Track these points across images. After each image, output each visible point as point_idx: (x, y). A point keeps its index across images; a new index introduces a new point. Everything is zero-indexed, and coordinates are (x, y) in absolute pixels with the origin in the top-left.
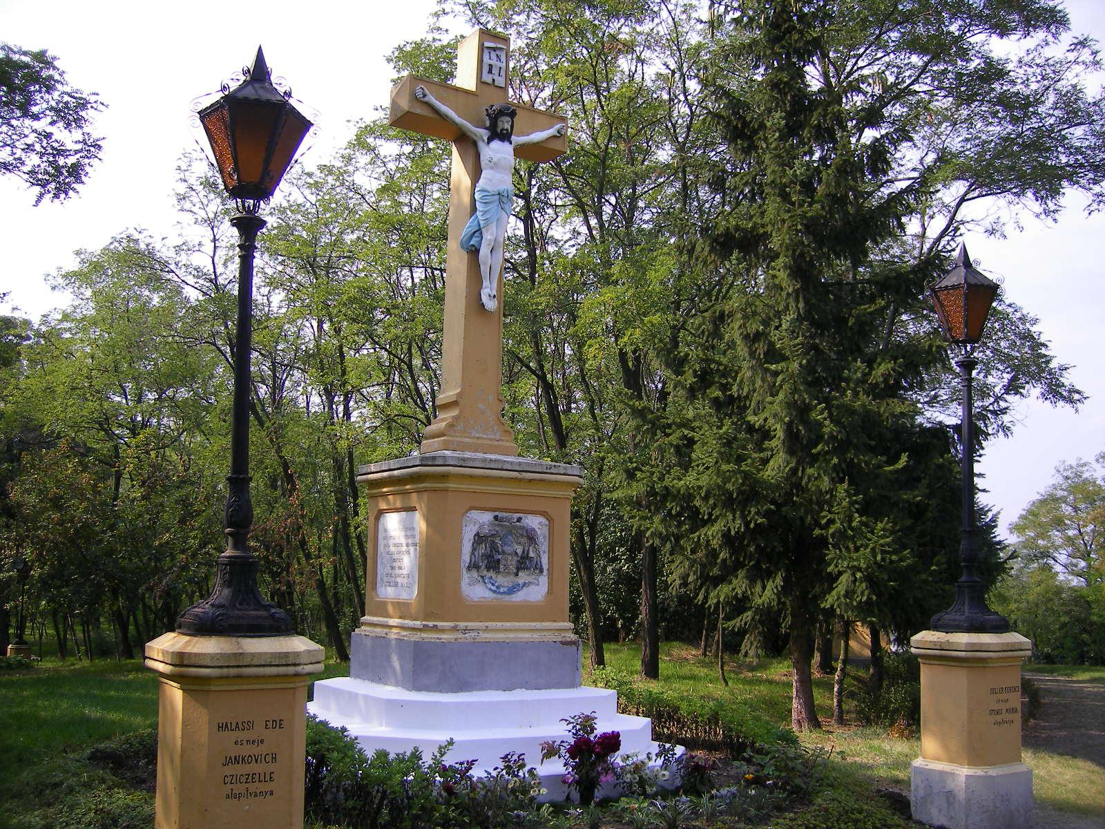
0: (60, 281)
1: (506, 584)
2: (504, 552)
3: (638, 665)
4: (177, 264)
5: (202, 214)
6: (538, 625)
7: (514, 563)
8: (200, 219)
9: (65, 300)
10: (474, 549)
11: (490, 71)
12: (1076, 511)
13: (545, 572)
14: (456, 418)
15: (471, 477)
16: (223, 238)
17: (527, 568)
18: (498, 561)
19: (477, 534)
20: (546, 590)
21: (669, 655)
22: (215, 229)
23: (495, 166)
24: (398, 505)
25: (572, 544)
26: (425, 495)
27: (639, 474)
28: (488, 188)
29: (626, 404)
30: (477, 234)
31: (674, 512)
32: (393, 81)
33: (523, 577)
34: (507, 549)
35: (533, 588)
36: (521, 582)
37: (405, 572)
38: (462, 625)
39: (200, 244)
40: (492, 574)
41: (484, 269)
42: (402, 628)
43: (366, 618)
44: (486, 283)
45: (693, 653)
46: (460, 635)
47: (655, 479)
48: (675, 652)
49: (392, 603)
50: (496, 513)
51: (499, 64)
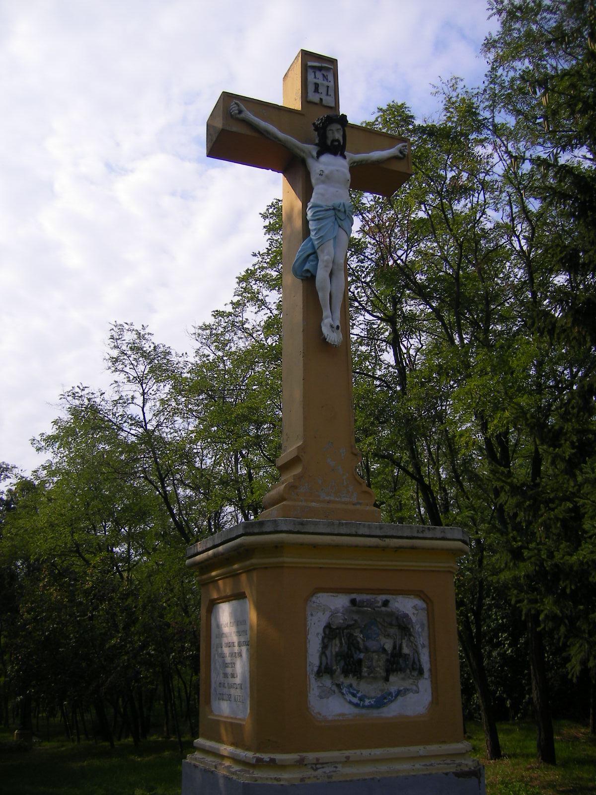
0: (43, 444)
1: (373, 694)
2: (367, 650)
3: (532, 746)
4: (114, 414)
5: (133, 373)
6: (420, 749)
7: (381, 663)
8: (132, 378)
9: (48, 456)
10: (325, 647)
11: (316, 90)
13: (426, 674)
14: (299, 478)
15: (315, 546)
16: (150, 391)
17: (401, 670)
18: (360, 661)
19: (328, 626)
20: (430, 699)
21: (559, 734)
22: (144, 386)
23: (327, 179)
24: (229, 592)
25: (459, 633)
26: (254, 574)
27: (526, 553)
28: (319, 203)
29: (503, 481)
30: (311, 258)
31: (568, 591)
33: (396, 682)
34: (372, 645)
35: (411, 697)
36: (393, 689)
37: (238, 680)
38: (311, 756)
39: (133, 398)
40: (351, 680)
41: (323, 297)
42: (236, 760)
43: (200, 741)
44: (326, 312)
45: (583, 730)
46: (310, 773)
47: (544, 557)
48: (565, 731)
49: (225, 722)
50: (354, 596)
51: (326, 83)
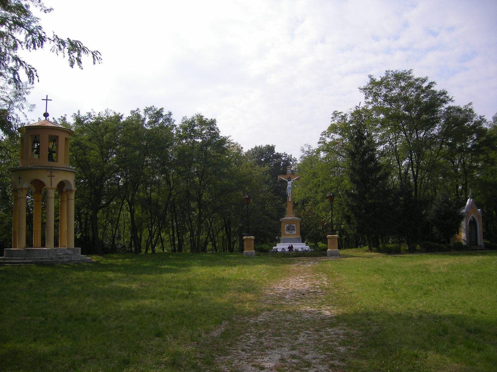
12: (152, 281)
32: (162, 109)
33: (293, 231)
